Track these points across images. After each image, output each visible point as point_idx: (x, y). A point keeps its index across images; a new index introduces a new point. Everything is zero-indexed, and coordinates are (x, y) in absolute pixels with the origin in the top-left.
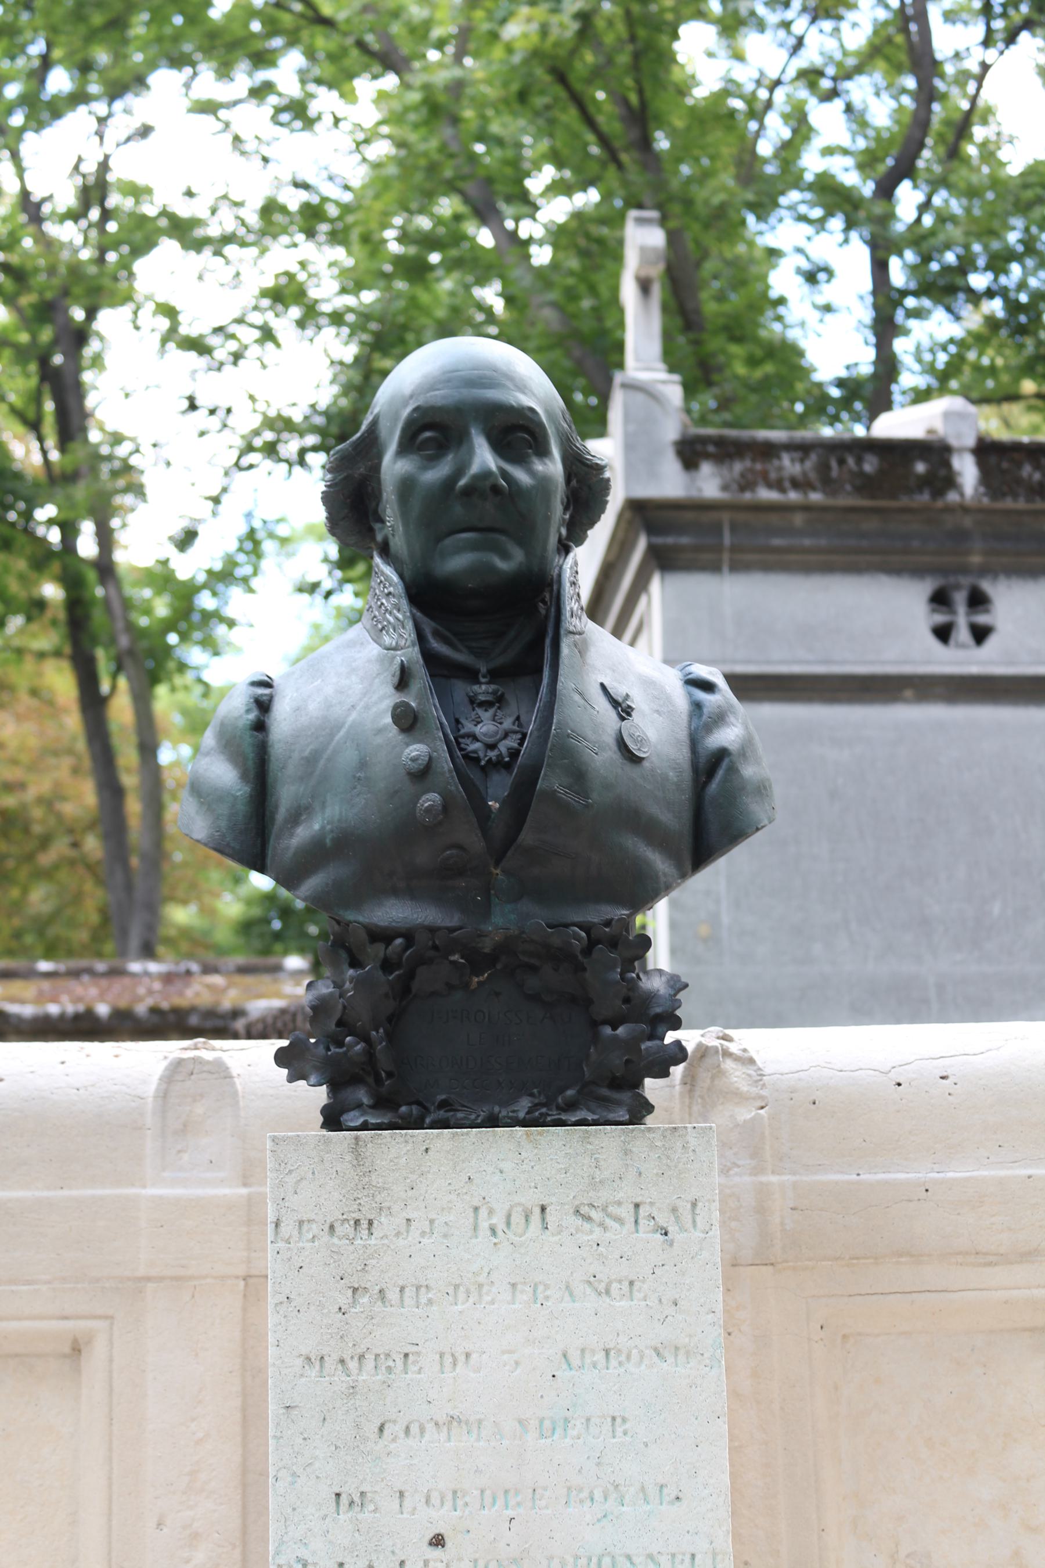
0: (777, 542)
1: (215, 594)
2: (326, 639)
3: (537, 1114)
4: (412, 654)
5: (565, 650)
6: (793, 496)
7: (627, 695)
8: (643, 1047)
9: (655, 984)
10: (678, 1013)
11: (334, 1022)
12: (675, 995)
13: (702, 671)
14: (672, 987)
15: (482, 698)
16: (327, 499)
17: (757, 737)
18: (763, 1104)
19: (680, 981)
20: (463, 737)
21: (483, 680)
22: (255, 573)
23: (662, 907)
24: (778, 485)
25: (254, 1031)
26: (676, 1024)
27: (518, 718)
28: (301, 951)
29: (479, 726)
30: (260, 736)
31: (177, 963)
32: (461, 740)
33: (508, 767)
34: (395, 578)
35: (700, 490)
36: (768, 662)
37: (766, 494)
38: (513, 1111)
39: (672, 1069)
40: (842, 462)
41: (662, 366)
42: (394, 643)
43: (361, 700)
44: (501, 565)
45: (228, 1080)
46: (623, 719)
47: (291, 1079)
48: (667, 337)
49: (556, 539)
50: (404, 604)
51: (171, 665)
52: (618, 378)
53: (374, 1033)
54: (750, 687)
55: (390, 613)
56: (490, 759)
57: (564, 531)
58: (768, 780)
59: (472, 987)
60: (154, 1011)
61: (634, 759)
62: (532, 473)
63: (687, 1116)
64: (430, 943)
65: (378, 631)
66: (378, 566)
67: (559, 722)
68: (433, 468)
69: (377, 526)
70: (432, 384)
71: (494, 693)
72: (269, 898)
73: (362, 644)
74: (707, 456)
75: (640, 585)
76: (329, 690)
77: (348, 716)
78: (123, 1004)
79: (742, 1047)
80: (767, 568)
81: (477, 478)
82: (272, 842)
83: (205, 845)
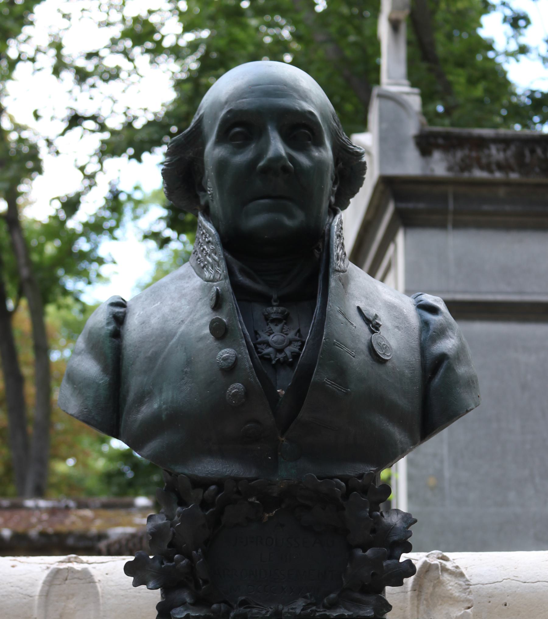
0: (486, 207)
1: (89, 240)
2: (166, 273)
3: (309, 610)
4: (223, 285)
5: (333, 283)
6: (498, 175)
7: (376, 315)
8: (384, 564)
9: (394, 520)
10: (409, 540)
11: (167, 545)
12: (408, 527)
13: (429, 299)
14: (405, 522)
15: (274, 316)
16: (165, 173)
17: (468, 348)
18: (469, 605)
19: (411, 517)
20: (260, 343)
21: (275, 304)
22: (117, 226)
23: (402, 463)
24: (488, 168)
25: (113, 549)
26: (408, 549)
27: (299, 331)
28: (147, 494)
29: (271, 336)
30: (116, 341)
31: (59, 501)
32: (258, 346)
33: (291, 365)
34: (213, 231)
35: (432, 170)
36: (479, 293)
37: (479, 174)
38: (292, 609)
39: (405, 580)
40: (533, 152)
41: (406, 82)
42: (212, 277)
43: (188, 316)
44: (288, 222)
45: (92, 584)
46: (373, 332)
47: (136, 584)
48: (411, 63)
49: (328, 204)
50: (219, 249)
51: (58, 290)
52: (376, 91)
53: (195, 552)
54: (462, 310)
55: (210, 256)
56: (279, 359)
57: (333, 199)
58: (475, 376)
59: (264, 521)
60: (43, 534)
61: (381, 361)
62: (311, 158)
63: (416, 613)
64: (235, 489)
65: (200, 269)
66: (201, 222)
67: (328, 334)
68: (241, 153)
69: (201, 194)
70: (240, 94)
71: (282, 313)
72: (125, 456)
73: (190, 277)
74: (438, 147)
75: (389, 238)
76: (166, 309)
77: (179, 328)
78: (20, 529)
79: (455, 565)
80: (480, 225)
81: (271, 160)
82: (124, 416)
83: (77, 418)
